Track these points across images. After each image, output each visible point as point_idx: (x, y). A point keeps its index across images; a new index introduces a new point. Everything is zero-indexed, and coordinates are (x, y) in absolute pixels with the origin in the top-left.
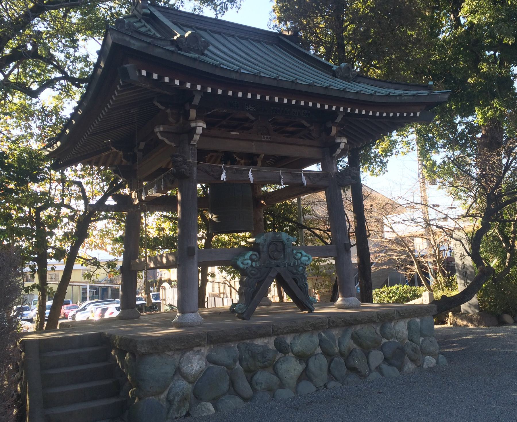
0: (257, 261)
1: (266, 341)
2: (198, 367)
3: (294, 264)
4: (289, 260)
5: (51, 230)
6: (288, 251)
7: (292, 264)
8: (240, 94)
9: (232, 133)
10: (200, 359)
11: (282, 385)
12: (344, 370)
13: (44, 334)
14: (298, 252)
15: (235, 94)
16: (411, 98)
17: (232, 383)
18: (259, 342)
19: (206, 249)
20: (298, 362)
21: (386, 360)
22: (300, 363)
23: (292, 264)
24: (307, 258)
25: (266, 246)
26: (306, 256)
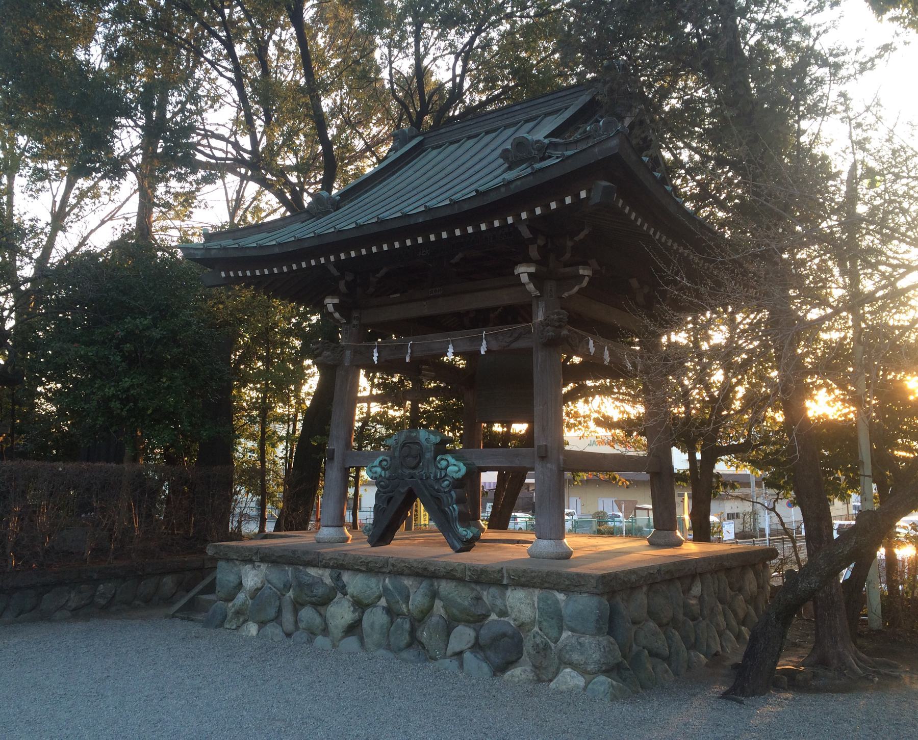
0: (387, 469)
1: (320, 572)
2: (252, 583)
3: (435, 476)
4: (428, 469)
5: (509, 427)
6: (427, 457)
7: (432, 476)
8: (397, 245)
9: (392, 296)
10: (256, 575)
11: (325, 631)
12: (406, 638)
13: (885, 573)
14: (442, 459)
15: (391, 246)
16: (531, 178)
17: (279, 611)
18: (312, 571)
19: (466, 450)
20: (352, 609)
21: (477, 646)
22: (353, 612)
23: (432, 476)
24: (456, 468)
25: (398, 449)
26: (455, 465)
